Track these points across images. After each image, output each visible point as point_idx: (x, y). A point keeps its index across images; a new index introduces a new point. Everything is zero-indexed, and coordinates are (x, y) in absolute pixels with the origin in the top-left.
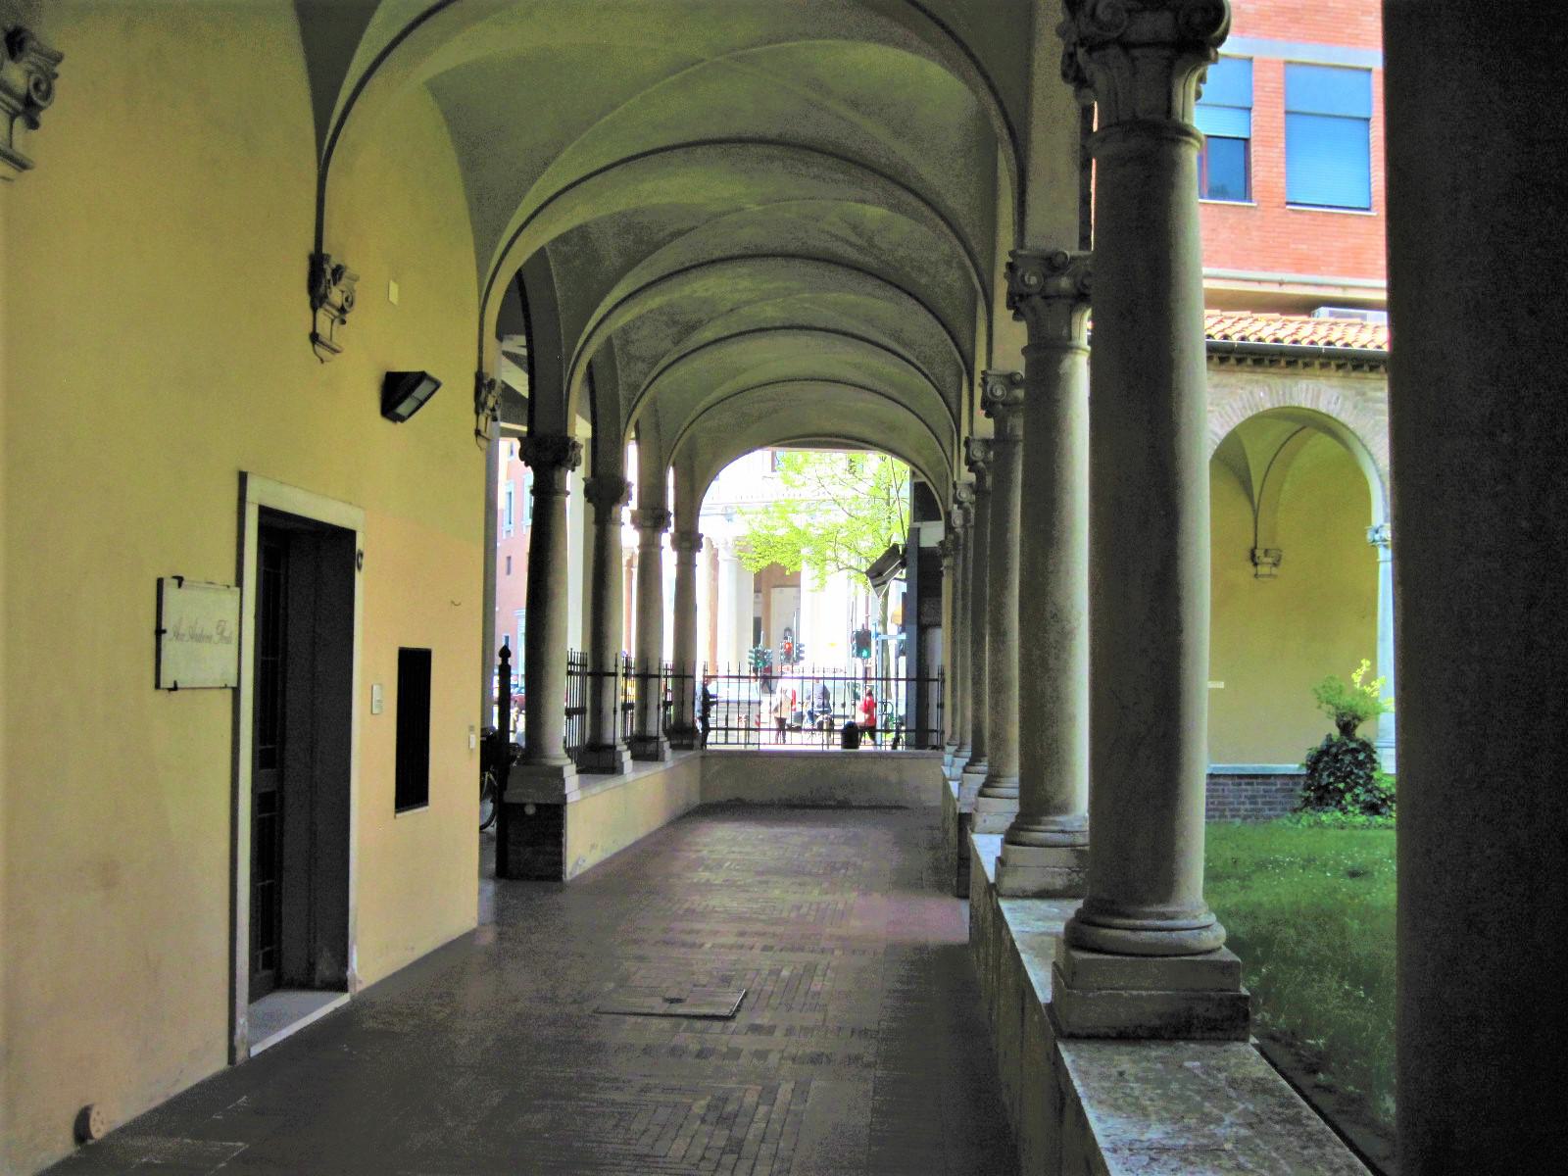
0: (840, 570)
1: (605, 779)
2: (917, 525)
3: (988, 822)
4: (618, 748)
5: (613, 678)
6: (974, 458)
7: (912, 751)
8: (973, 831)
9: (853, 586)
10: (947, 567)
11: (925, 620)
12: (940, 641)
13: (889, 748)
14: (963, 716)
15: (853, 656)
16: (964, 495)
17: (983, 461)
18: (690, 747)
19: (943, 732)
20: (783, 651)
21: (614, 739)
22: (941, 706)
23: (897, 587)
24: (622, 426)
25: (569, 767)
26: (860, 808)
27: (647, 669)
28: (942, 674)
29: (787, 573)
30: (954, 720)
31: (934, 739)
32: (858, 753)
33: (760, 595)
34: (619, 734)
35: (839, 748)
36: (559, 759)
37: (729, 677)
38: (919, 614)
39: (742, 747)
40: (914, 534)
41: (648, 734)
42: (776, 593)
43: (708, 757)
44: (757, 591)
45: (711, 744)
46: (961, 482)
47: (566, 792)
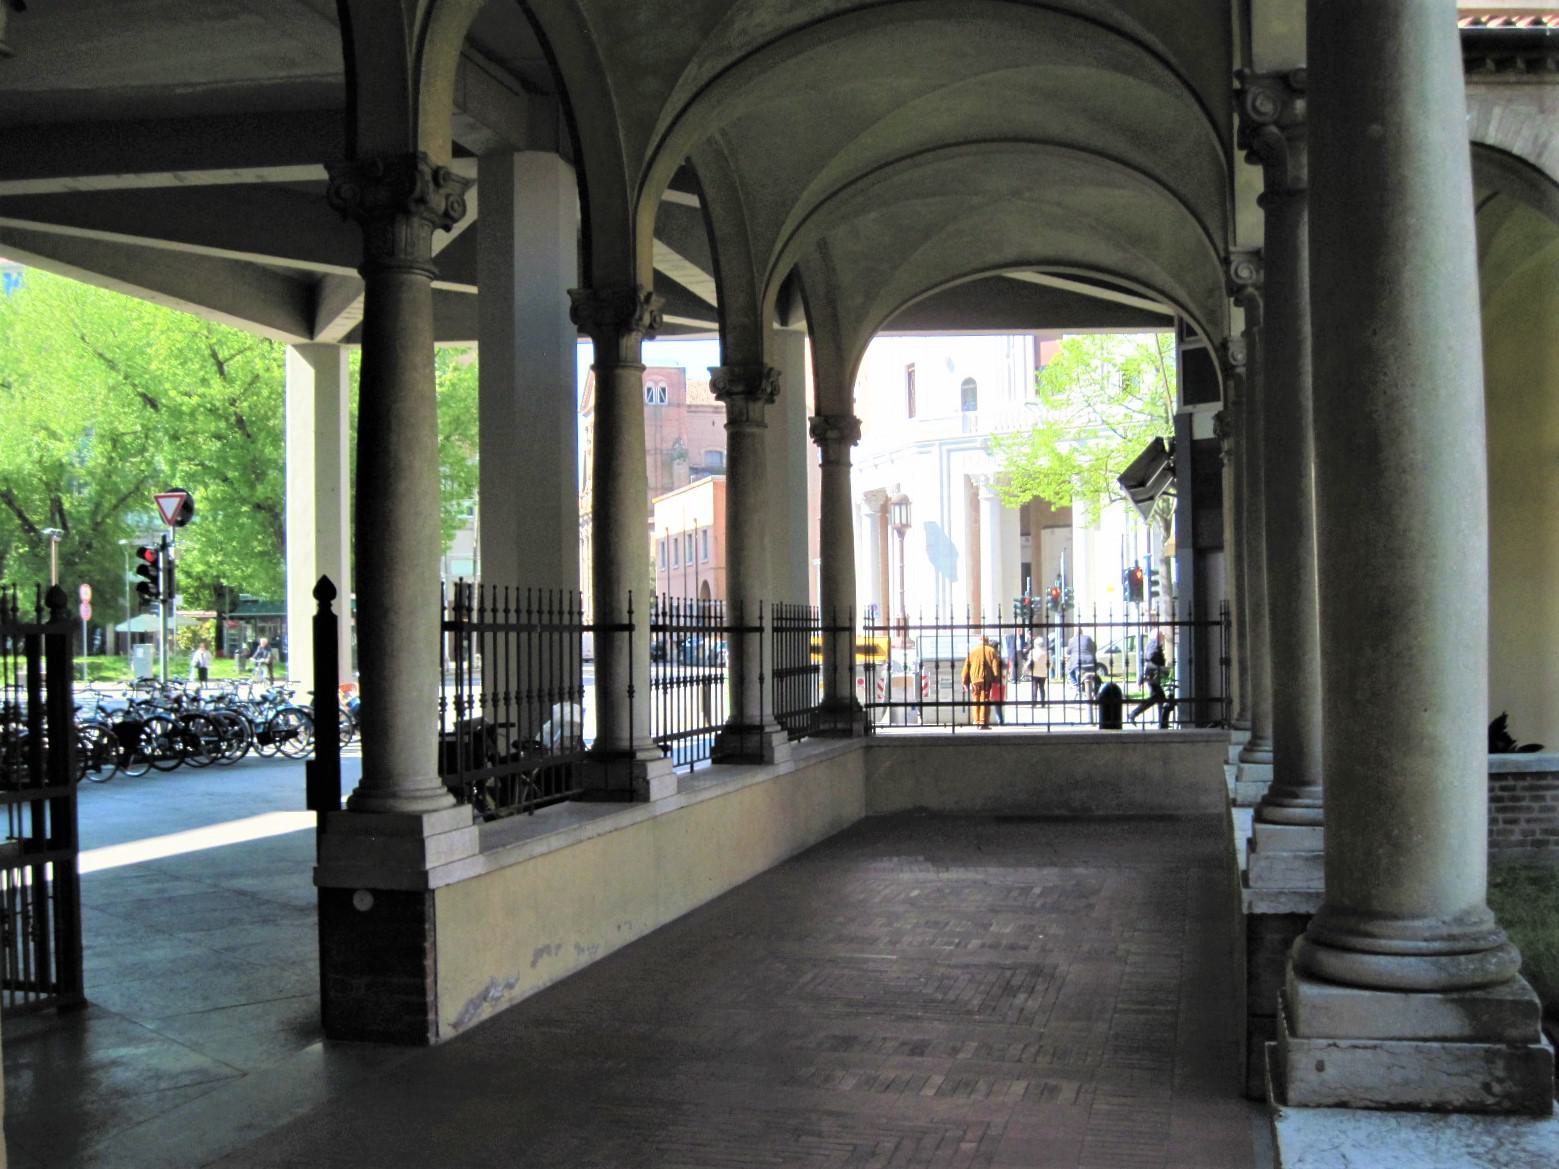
0: (1112, 501)
1: (616, 811)
2: (1189, 408)
3: (1330, 1072)
4: (767, 730)
5: (758, 634)
6: (1255, 117)
7: (1192, 730)
8: (1283, 1100)
9: (1131, 522)
10: (1228, 453)
11: (1204, 542)
12: (1223, 566)
13: (1156, 727)
14: (1257, 686)
15: (1125, 599)
16: (1244, 273)
17: (1276, 123)
18: (848, 733)
19: (1230, 702)
20: (1049, 597)
21: (761, 715)
22: (1226, 662)
23: (1169, 500)
24: (631, 195)
25: (781, 747)
26: (1106, 820)
27: (835, 620)
28: (1227, 614)
29: (1053, 509)
30: (1242, 686)
31: (1218, 711)
32: (1120, 736)
33: (1030, 538)
34: (768, 710)
35: (1096, 729)
36: (415, 798)
37: (937, 627)
38: (1196, 535)
39: (948, 731)
40: (1183, 422)
41: (747, 721)
42: (1046, 535)
43: (879, 748)
44: (1025, 533)
45: (882, 727)
46: (1239, 249)
47: (428, 866)
